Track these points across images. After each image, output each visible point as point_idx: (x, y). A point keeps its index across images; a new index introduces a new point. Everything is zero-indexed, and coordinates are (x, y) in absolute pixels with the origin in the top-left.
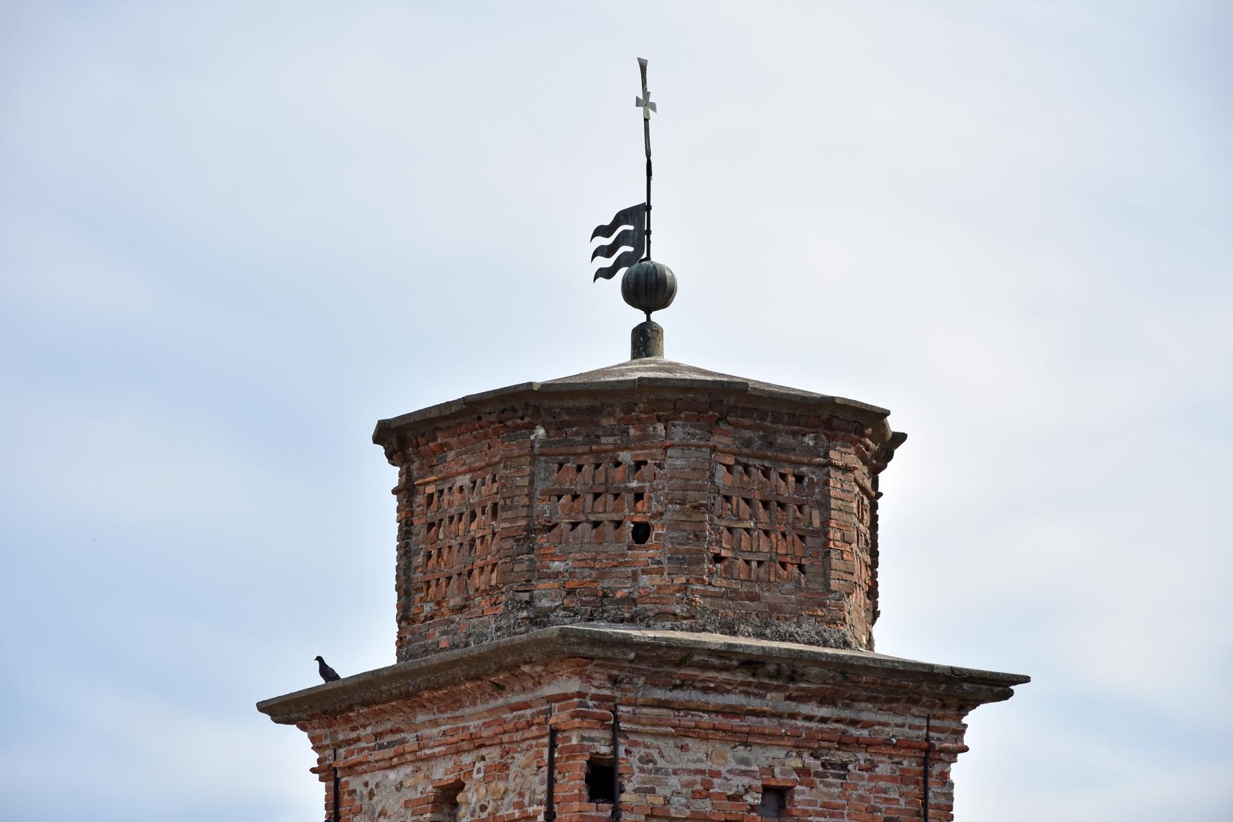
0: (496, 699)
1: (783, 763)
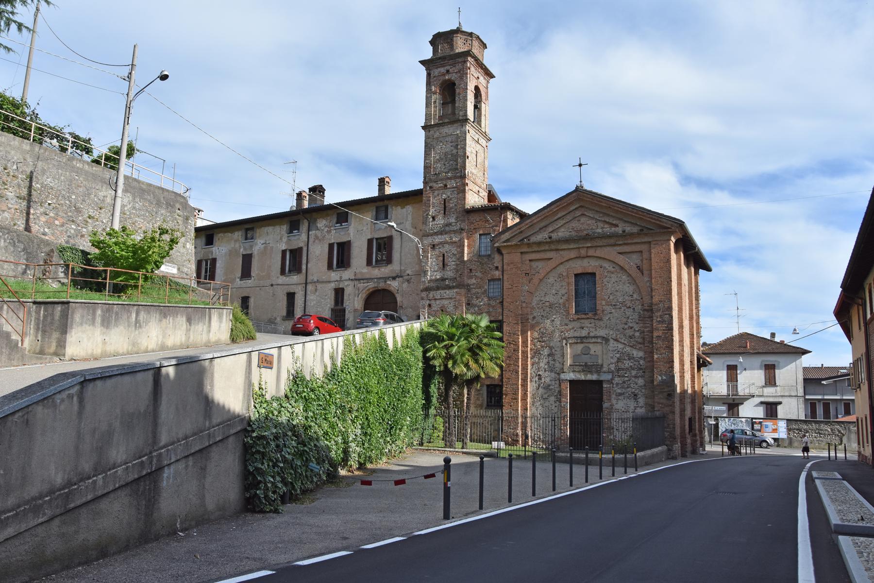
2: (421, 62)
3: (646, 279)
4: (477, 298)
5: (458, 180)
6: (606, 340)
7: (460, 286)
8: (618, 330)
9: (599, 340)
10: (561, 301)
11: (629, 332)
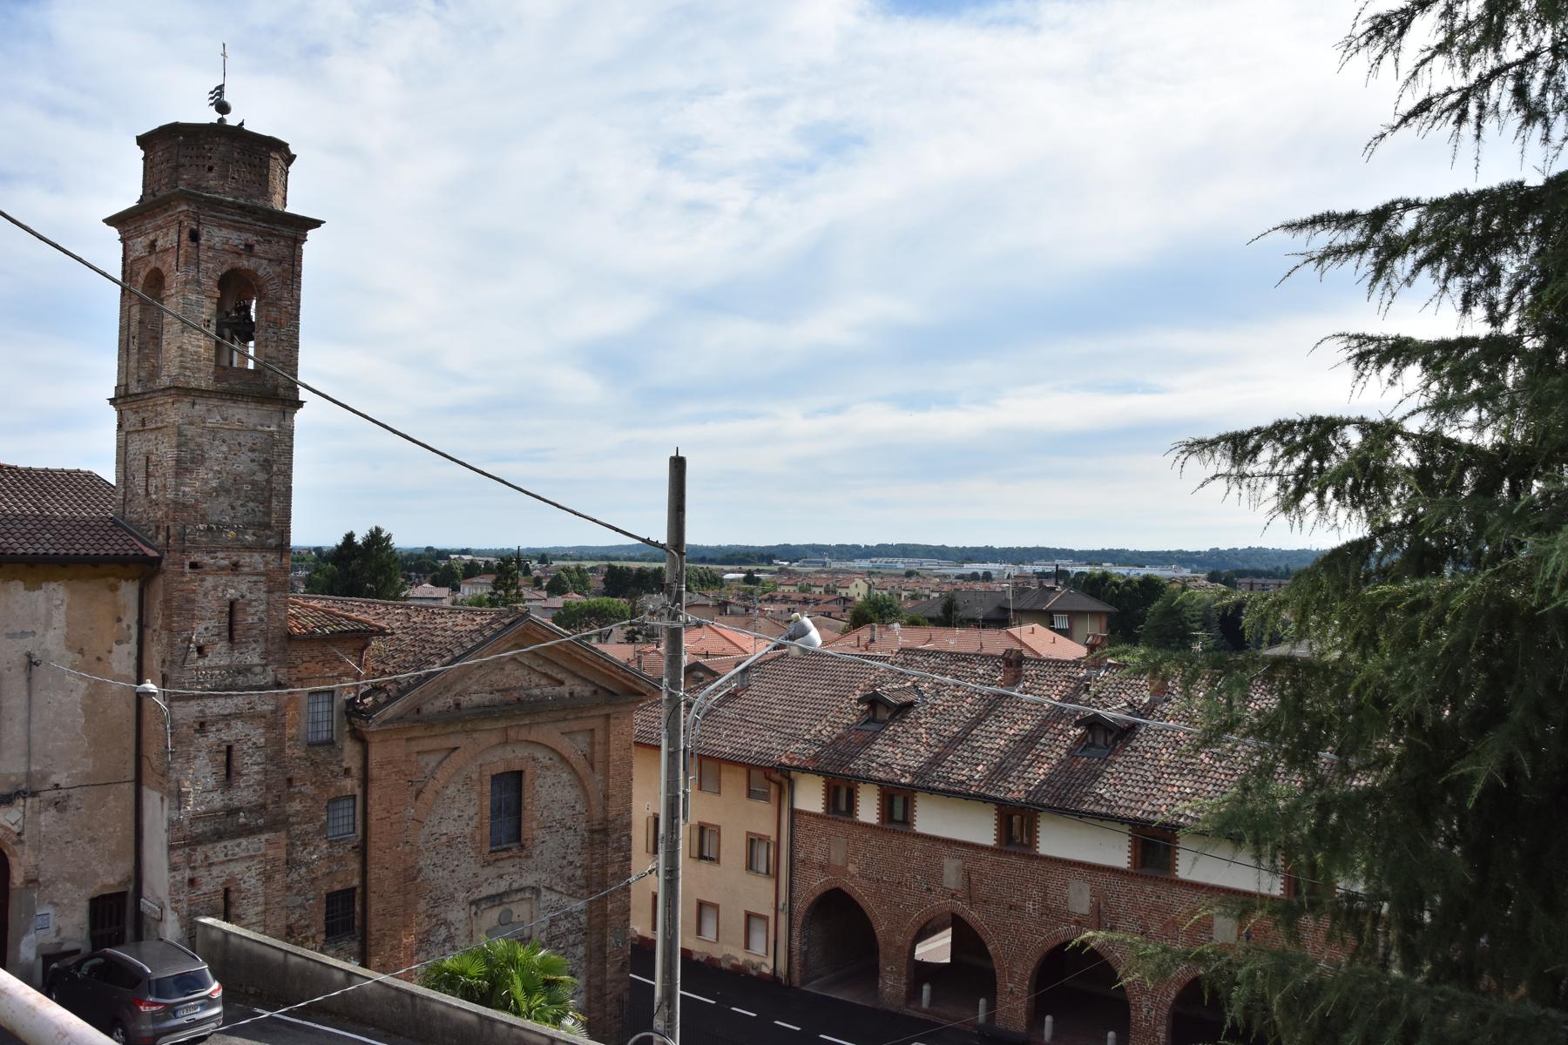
0: (565, 570)
1: (252, 238)
2: (110, 221)
3: (599, 777)
4: (305, 845)
5: (271, 556)
6: (536, 890)
7: (272, 826)
8: (553, 871)
9: (528, 895)
10: (467, 831)
11: (568, 871)
